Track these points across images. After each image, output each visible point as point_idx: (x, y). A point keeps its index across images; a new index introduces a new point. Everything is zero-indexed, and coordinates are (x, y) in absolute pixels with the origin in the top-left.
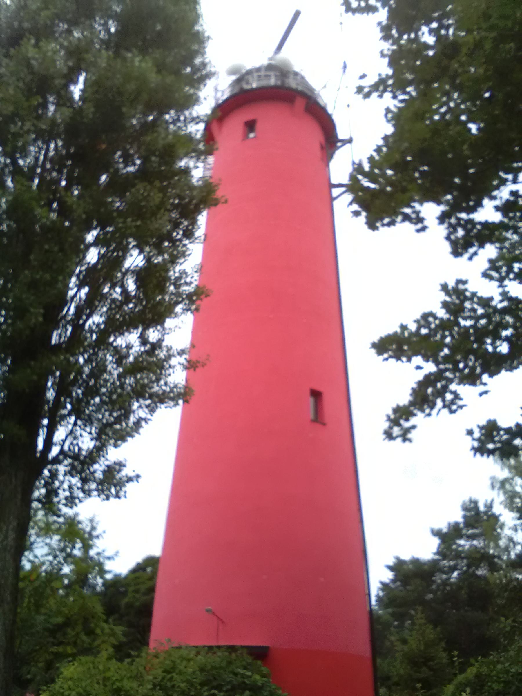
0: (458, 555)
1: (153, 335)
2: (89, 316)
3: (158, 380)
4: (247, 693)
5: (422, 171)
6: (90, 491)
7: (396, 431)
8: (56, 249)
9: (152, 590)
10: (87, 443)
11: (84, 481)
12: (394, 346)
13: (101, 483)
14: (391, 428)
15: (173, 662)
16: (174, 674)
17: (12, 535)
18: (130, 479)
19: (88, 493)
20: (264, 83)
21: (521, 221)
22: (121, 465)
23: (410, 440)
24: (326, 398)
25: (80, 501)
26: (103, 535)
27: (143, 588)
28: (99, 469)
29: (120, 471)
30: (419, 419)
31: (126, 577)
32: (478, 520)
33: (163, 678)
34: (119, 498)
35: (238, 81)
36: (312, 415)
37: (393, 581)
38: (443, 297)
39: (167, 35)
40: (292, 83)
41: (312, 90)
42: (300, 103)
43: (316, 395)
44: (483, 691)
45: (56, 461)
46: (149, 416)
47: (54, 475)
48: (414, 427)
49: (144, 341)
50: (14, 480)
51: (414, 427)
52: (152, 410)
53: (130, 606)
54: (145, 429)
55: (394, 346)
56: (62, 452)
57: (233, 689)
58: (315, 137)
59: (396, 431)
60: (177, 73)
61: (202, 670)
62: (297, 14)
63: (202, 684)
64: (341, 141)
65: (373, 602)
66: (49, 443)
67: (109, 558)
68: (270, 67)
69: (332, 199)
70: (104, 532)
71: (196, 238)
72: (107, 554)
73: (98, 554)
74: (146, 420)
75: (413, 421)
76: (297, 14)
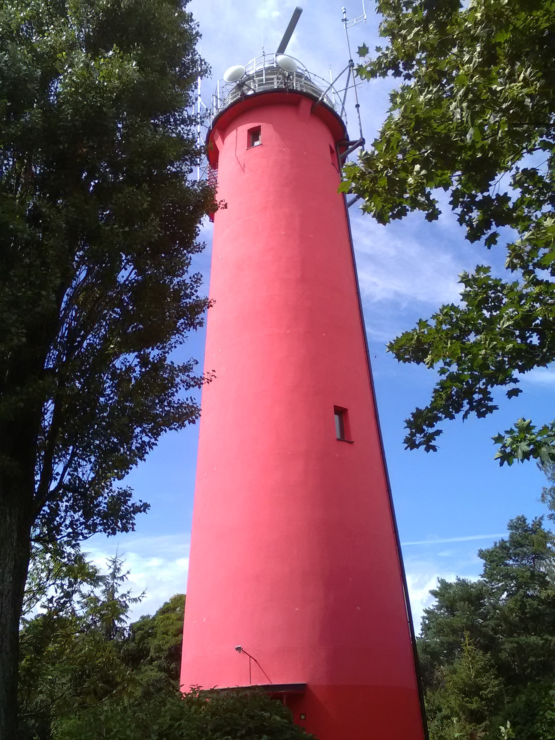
0: (507, 576)
1: (154, 353)
2: (84, 338)
3: (161, 402)
4: (265, 737)
5: (433, 159)
6: (95, 525)
7: (419, 438)
8: (38, 262)
9: (180, 631)
10: (86, 472)
11: (87, 515)
12: (413, 349)
13: (104, 516)
14: (413, 435)
15: (182, 708)
16: (183, 721)
17: (9, 578)
18: (137, 510)
19: (93, 529)
20: (268, 87)
21: (454, 1)
22: (125, 495)
23: (434, 448)
24: (352, 415)
25: (86, 538)
26: (127, 575)
27: (172, 629)
28: (103, 501)
29: (125, 502)
30: (443, 424)
31: (154, 619)
32: (525, 538)
33: (171, 726)
34: (127, 531)
35: (240, 86)
36: (338, 436)
37: (439, 608)
38: (462, 288)
39: (160, 42)
40: (296, 85)
41: (319, 92)
42: (305, 106)
43: (341, 412)
44: (535, 721)
45: (55, 496)
46: (153, 440)
47: (55, 512)
48: (438, 432)
49: (144, 361)
50: (8, 518)
51: (438, 432)
52: (156, 434)
53: (159, 649)
54: (151, 455)
55: (413, 349)
56: (61, 485)
57: (249, 732)
58: (324, 139)
59: (419, 438)
60: (163, 72)
61: (214, 714)
62: (298, 13)
63: (214, 731)
64: (353, 143)
65: (418, 631)
66: (48, 476)
67: (135, 600)
68: (271, 71)
69: (347, 206)
70: (128, 573)
71: (195, 247)
72: (132, 596)
73: (123, 596)
74: (151, 445)
75: (438, 426)
76: (298, 13)
